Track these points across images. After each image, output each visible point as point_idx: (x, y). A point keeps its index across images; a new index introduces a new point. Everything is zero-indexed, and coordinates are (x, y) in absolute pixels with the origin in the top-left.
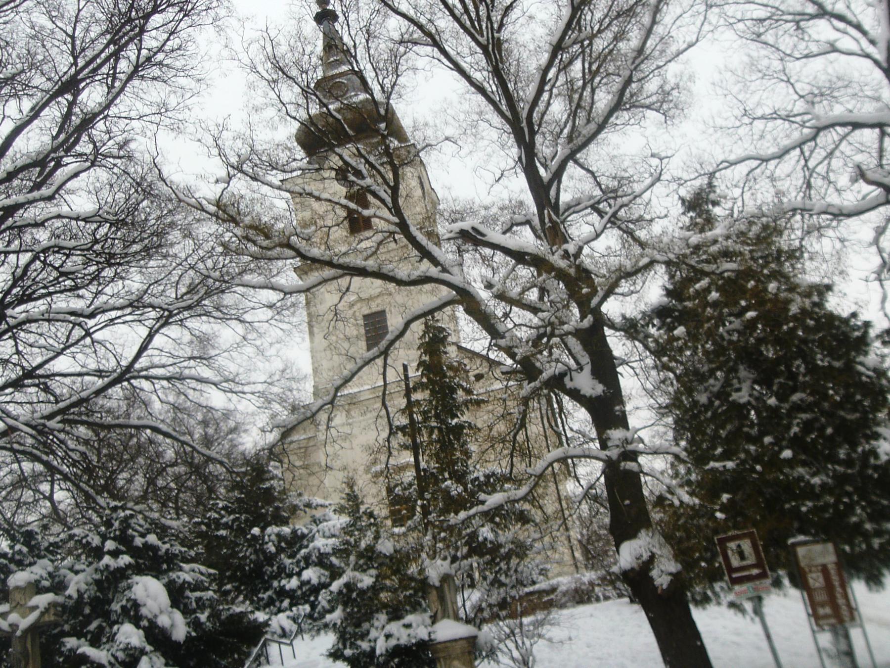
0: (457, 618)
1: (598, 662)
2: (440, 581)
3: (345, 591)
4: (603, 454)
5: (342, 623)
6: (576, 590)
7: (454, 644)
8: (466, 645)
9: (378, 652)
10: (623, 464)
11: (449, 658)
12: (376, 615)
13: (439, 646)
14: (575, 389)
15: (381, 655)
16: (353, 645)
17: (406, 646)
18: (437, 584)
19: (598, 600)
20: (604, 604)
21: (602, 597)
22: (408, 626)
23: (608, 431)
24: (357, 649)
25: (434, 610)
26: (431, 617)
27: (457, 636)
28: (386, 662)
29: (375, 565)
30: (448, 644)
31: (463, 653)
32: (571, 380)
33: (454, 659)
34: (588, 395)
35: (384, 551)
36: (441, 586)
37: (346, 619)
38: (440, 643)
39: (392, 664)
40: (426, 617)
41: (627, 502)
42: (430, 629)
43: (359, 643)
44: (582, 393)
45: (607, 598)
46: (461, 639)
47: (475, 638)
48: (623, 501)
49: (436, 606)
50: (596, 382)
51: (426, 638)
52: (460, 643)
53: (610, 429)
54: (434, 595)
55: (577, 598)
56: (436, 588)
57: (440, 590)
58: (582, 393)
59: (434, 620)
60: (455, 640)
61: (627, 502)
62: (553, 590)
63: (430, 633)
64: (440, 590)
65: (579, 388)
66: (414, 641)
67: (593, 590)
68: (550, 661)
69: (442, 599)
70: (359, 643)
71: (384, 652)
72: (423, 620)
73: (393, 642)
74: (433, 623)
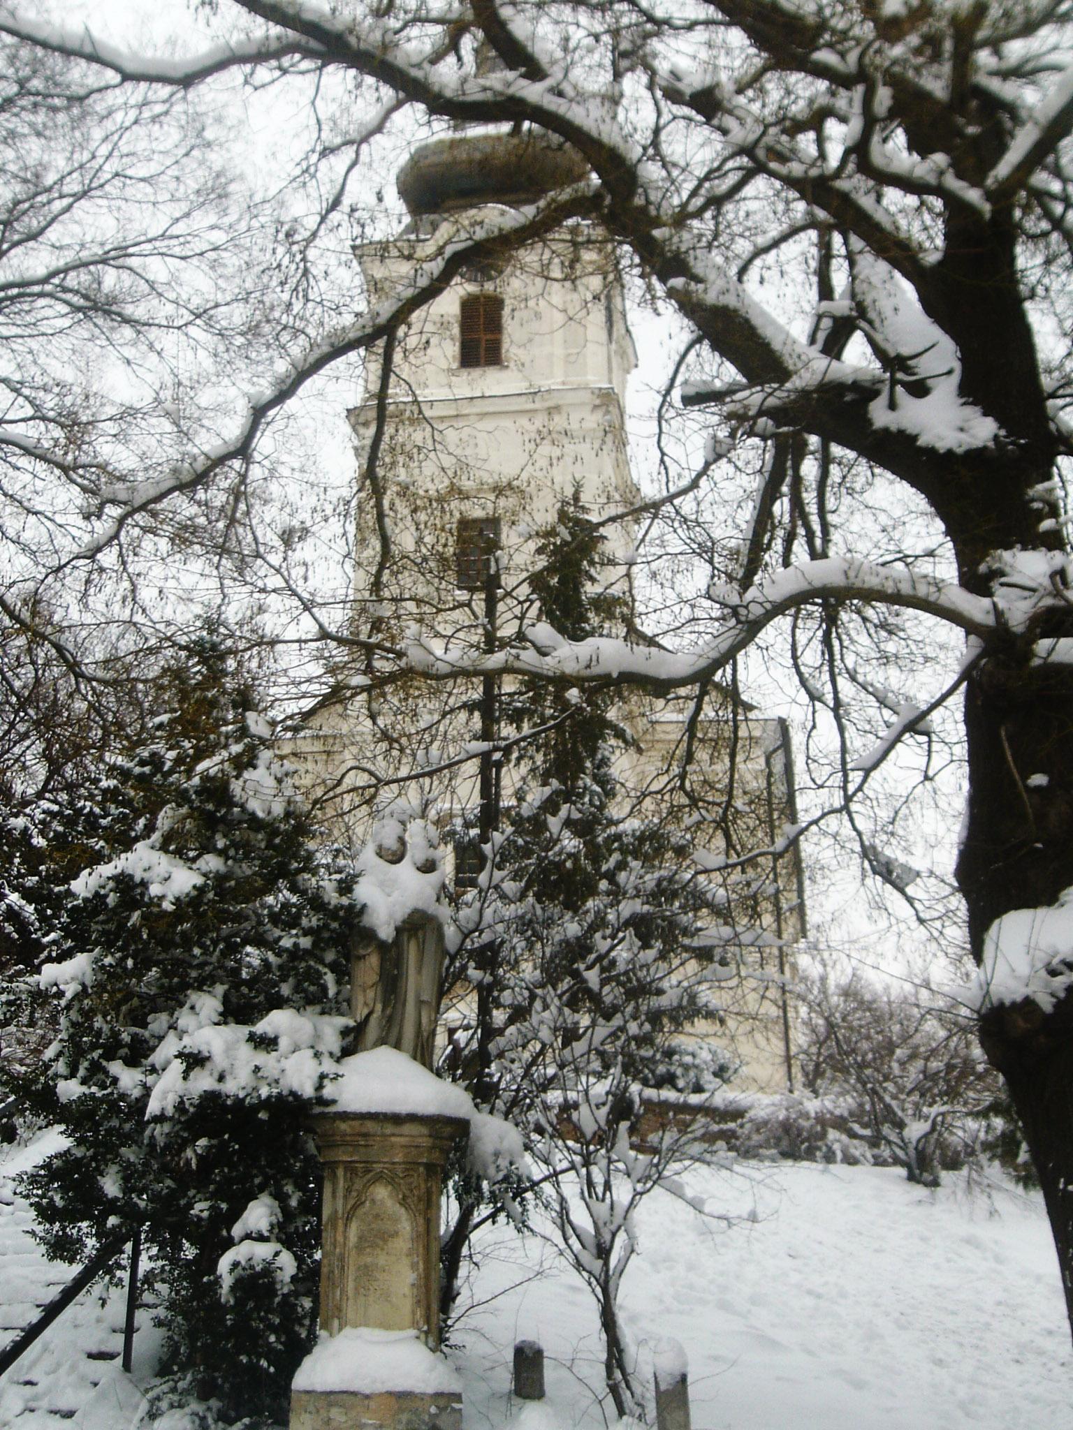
0: (423, 1053)
1: (809, 1301)
2: (398, 930)
3: (112, 899)
4: (977, 607)
5: (77, 997)
6: (786, 1126)
7: (389, 1129)
8: (426, 1142)
9: (153, 1107)
10: (1043, 645)
11: (363, 1172)
12: (194, 997)
13: (343, 1126)
14: (901, 432)
15: (160, 1119)
16: (96, 1073)
17: (239, 1102)
18: (386, 933)
19: (829, 1158)
20: (839, 1169)
21: (839, 1155)
22: (266, 1043)
23: (1006, 555)
24: (103, 1087)
25: (361, 1012)
26: (345, 1032)
27: (403, 1107)
28: (177, 1145)
29: (221, 843)
30: (370, 1126)
31: (411, 1165)
32: (892, 406)
33: (379, 1178)
34: (942, 446)
35: (255, 806)
36: (397, 941)
37: (100, 987)
38: (345, 1116)
39: (189, 1153)
40: (331, 1029)
41: (1039, 780)
42: (328, 1066)
43: (116, 1068)
44: (921, 442)
45: (851, 1161)
46: (413, 1118)
47: (461, 1127)
48: (1025, 777)
49: (366, 1000)
50: (973, 413)
51: (308, 1091)
52: (408, 1129)
53: (1008, 546)
54: (369, 968)
55: (785, 1143)
56: (382, 946)
57: (391, 954)
58: (921, 442)
59: (352, 1043)
60: (397, 1119)
61: (1039, 780)
62: (736, 1114)
63: (322, 1077)
64: (391, 954)
65: (911, 430)
66: (264, 1092)
67: (823, 1135)
68: (691, 1267)
69: (391, 985)
70: (116, 1068)
71: (170, 1111)
72: (317, 1036)
73: (203, 1082)
74: (347, 1052)
